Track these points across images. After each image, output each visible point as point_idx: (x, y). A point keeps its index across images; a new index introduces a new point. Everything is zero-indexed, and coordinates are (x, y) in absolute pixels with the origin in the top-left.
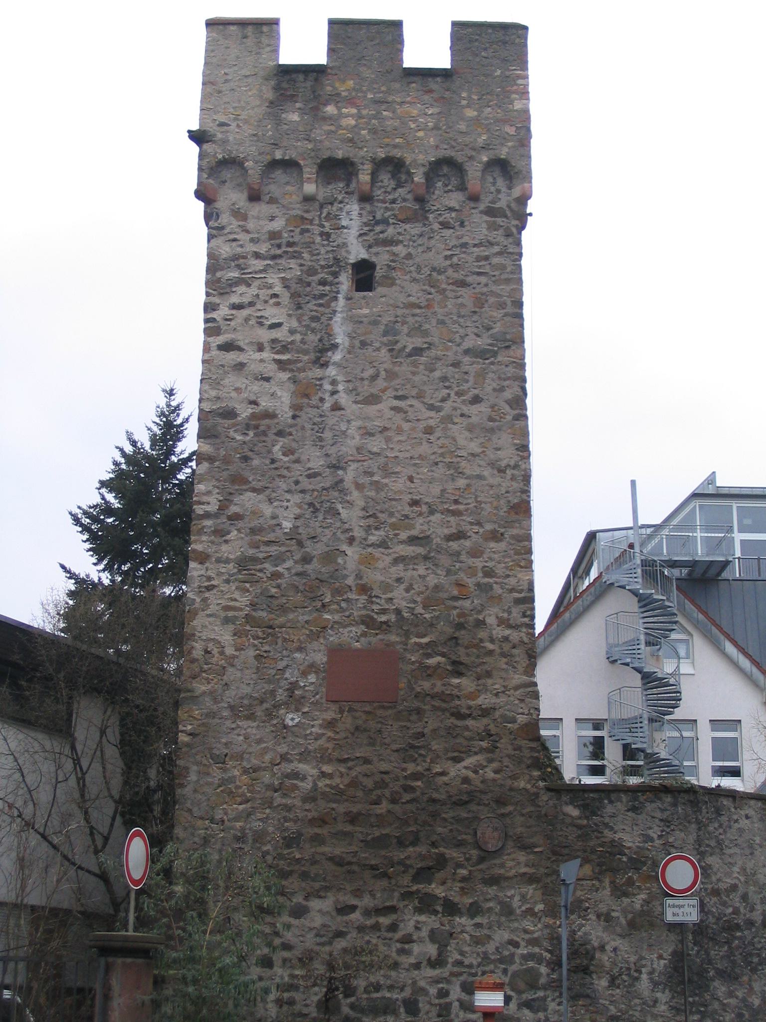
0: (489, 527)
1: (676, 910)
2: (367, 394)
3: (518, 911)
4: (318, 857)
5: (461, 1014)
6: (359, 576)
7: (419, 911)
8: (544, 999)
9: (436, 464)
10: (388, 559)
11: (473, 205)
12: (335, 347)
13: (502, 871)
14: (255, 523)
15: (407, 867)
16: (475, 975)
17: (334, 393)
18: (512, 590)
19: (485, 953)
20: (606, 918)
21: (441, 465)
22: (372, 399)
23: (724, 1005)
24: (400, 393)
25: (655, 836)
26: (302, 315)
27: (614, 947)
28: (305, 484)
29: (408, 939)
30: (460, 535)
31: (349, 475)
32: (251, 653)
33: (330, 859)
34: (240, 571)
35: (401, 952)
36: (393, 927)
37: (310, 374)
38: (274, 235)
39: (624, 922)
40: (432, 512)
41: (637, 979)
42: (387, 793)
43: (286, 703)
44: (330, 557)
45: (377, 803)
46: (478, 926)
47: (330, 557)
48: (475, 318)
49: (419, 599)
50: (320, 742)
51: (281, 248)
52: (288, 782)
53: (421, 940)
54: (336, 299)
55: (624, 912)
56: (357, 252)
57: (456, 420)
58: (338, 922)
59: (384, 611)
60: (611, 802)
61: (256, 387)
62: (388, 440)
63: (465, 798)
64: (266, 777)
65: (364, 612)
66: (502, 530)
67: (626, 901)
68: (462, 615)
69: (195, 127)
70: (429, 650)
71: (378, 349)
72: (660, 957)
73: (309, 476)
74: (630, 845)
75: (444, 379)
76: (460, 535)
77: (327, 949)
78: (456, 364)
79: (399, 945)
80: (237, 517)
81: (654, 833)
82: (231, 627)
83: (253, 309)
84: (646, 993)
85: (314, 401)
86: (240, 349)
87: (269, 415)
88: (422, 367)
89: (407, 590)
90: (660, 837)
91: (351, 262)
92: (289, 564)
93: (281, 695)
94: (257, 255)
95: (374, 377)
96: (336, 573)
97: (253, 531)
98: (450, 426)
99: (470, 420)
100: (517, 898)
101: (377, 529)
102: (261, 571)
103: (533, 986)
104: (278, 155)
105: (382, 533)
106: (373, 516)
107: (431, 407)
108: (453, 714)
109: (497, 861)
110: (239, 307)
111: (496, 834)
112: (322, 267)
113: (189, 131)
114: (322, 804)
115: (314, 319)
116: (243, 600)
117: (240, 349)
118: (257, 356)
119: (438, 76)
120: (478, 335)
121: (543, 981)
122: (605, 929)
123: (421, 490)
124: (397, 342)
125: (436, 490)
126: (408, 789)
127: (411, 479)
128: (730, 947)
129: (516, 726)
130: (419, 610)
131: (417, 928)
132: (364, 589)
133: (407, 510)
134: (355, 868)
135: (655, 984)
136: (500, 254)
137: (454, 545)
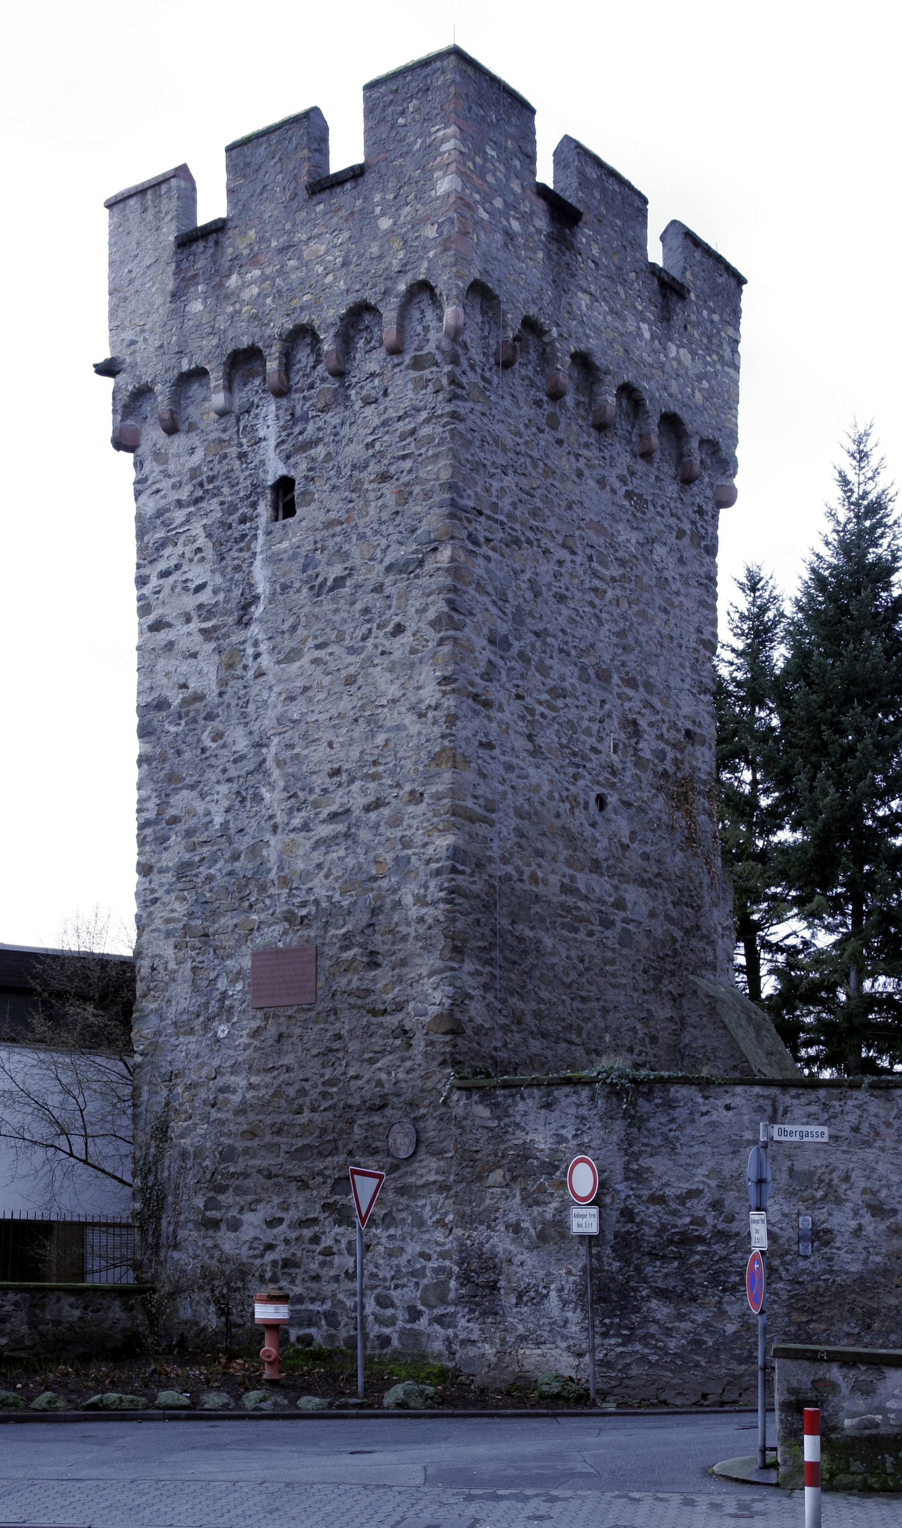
0: (408, 787)
1: (580, 1220)
2: (287, 650)
3: (430, 1222)
4: (249, 1170)
5: (376, 1328)
6: (281, 868)
7: (339, 1222)
8: (454, 1315)
9: (356, 720)
10: (309, 844)
11: (396, 361)
12: (256, 598)
13: (413, 1179)
14: (192, 823)
15: (326, 1177)
16: (389, 1288)
17: (257, 656)
18: (428, 862)
19: (398, 1266)
20: (516, 1228)
21: (361, 720)
22: (293, 655)
23: (667, 1329)
24: (320, 641)
25: (570, 1136)
26: (226, 567)
27: (526, 1264)
28: (233, 772)
29: (328, 1252)
30: (378, 804)
31: (270, 753)
32: (189, 965)
33: (259, 1171)
34: (178, 879)
35: (323, 1264)
36: (315, 1240)
37: (234, 639)
38: (194, 472)
39: (533, 1232)
40: (352, 781)
41: (546, 1296)
42: (307, 1100)
43: (217, 1015)
44: (254, 850)
45: (299, 1112)
46: (391, 1237)
47: (254, 850)
48: (399, 519)
49: (337, 885)
50: (248, 1053)
51: (203, 487)
52: (221, 1097)
53: (340, 1253)
54: (255, 536)
55: (534, 1222)
56: (275, 469)
57: (376, 661)
58: (268, 1236)
59: (304, 904)
60: (523, 1098)
61: (184, 668)
62: (310, 700)
63: (378, 1102)
64: (203, 1093)
65: (285, 908)
66: (421, 789)
67: (536, 1209)
68: (380, 897)
69: (104, 354)
70: (347, 941)
71: (299, 591)
72: (569, 1273)
73: (235, 761)
74: (542, 1146)
75: (366, 610)
76: (378, 804)
77: (258, 1262)
78: (379, 589)
79: (321, 1258)
80: (175, 820)
81: (568, 1133)
82: (172, 941)
83: (179, 572)
84: (556, 1313)
85: (239, 672)
86: (169, 625)
87: (198, 697)
88: (342, 601)
89: (326, 877)
90: (575, 1136)
91: (270, 483)
92: (219, 865)
93: (214, 1007)
94: (180, 504)
95: (294, 628)
96: (261, 868)
97: (189, 833)
98: (370, 670)
99: (392, 657)
100: (428, 1208)
101: (299, 810)
102: (196, 876)
103: (443, 1301)
104: (185, 368)
105: (303, 814)
106: (295, 795)
107: (352, 651)
108: (368, 1012)
109: (408, 1169)
110: (165, 574)
111: (407, 1140)
112: (242, 500)
113: (95, 366)
114: (252, 1116)
115: (237, 569)
116: (181, 909)
117: (169, 625)
118: (186, 629)
119: (345, 181)
120: (401, 543)
121: (452, 1295)
122: (513, 1241)
123: (342, 755)
124: (317, 576)
125: (355, 753)
126: (324, 1095)
127: (330, 745)
128: (682, 1264)
129: (428, 1019)
130: (337, 897)
131: (337, 1241)
132: (285, 881)
133: (329, 783)
134: (281, 1180)
135: (565, 1303)
136: (427, 421)
137: (373, 816)
